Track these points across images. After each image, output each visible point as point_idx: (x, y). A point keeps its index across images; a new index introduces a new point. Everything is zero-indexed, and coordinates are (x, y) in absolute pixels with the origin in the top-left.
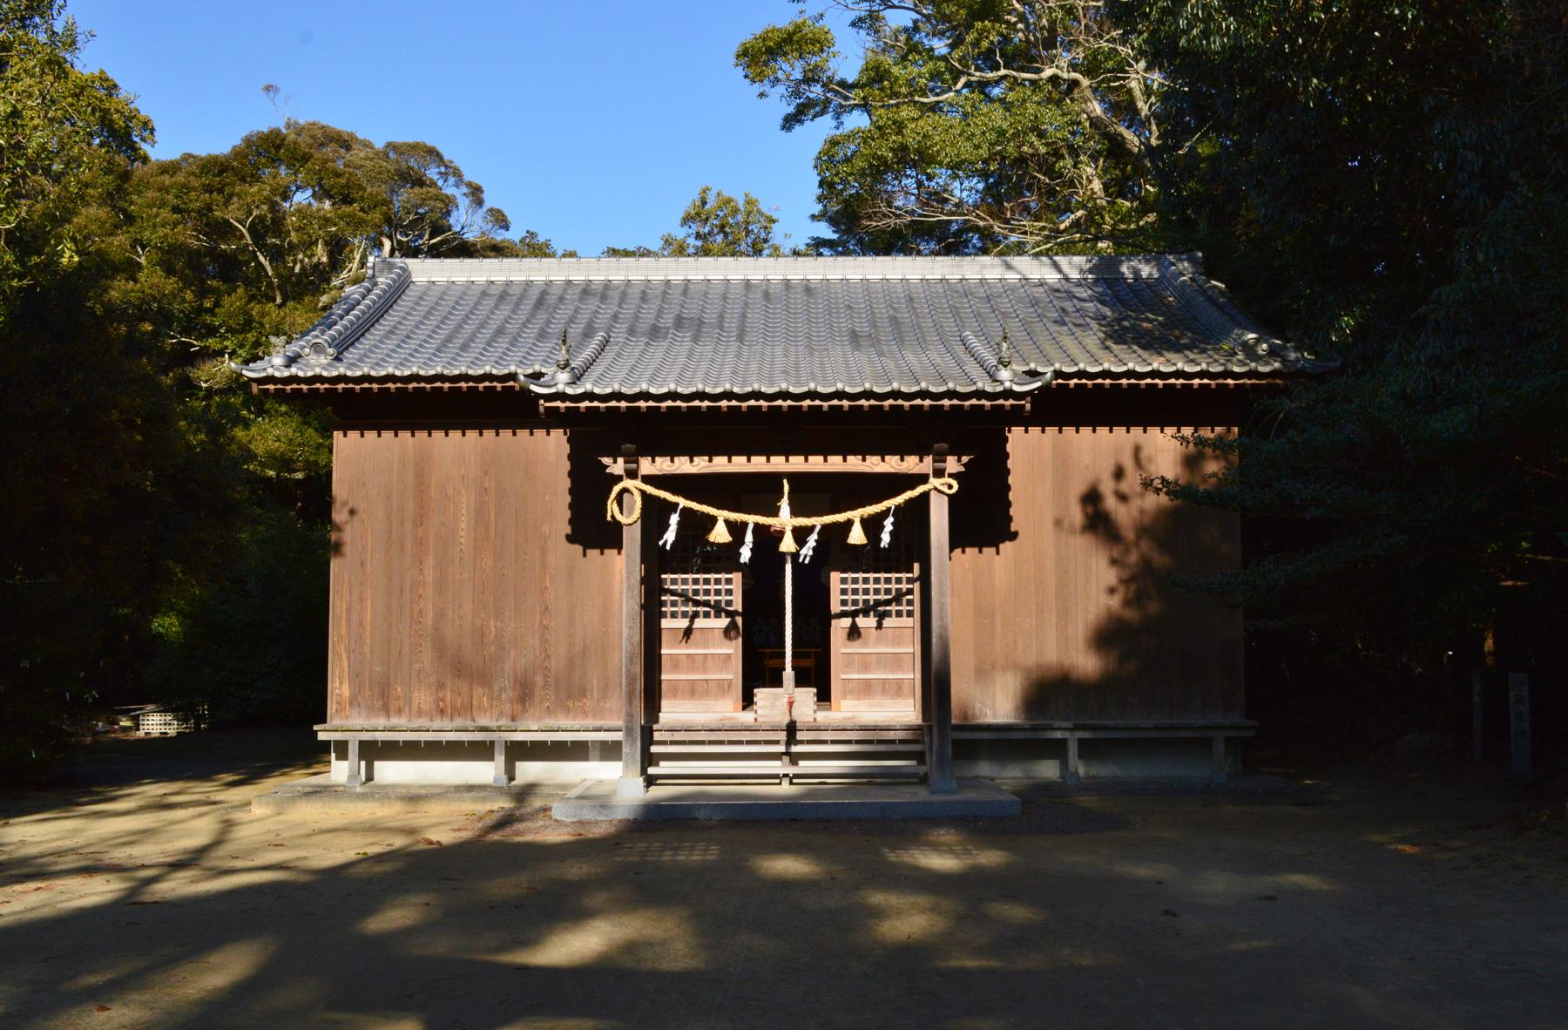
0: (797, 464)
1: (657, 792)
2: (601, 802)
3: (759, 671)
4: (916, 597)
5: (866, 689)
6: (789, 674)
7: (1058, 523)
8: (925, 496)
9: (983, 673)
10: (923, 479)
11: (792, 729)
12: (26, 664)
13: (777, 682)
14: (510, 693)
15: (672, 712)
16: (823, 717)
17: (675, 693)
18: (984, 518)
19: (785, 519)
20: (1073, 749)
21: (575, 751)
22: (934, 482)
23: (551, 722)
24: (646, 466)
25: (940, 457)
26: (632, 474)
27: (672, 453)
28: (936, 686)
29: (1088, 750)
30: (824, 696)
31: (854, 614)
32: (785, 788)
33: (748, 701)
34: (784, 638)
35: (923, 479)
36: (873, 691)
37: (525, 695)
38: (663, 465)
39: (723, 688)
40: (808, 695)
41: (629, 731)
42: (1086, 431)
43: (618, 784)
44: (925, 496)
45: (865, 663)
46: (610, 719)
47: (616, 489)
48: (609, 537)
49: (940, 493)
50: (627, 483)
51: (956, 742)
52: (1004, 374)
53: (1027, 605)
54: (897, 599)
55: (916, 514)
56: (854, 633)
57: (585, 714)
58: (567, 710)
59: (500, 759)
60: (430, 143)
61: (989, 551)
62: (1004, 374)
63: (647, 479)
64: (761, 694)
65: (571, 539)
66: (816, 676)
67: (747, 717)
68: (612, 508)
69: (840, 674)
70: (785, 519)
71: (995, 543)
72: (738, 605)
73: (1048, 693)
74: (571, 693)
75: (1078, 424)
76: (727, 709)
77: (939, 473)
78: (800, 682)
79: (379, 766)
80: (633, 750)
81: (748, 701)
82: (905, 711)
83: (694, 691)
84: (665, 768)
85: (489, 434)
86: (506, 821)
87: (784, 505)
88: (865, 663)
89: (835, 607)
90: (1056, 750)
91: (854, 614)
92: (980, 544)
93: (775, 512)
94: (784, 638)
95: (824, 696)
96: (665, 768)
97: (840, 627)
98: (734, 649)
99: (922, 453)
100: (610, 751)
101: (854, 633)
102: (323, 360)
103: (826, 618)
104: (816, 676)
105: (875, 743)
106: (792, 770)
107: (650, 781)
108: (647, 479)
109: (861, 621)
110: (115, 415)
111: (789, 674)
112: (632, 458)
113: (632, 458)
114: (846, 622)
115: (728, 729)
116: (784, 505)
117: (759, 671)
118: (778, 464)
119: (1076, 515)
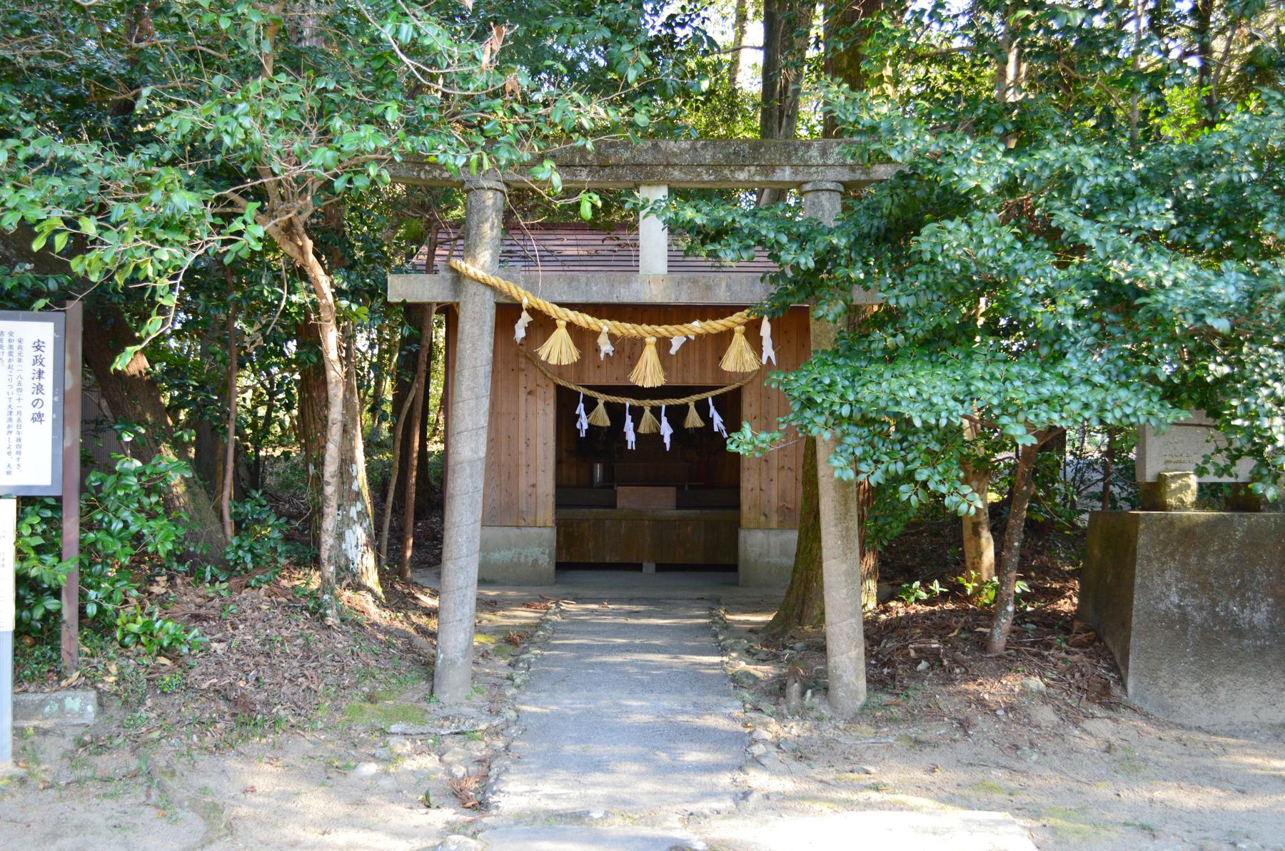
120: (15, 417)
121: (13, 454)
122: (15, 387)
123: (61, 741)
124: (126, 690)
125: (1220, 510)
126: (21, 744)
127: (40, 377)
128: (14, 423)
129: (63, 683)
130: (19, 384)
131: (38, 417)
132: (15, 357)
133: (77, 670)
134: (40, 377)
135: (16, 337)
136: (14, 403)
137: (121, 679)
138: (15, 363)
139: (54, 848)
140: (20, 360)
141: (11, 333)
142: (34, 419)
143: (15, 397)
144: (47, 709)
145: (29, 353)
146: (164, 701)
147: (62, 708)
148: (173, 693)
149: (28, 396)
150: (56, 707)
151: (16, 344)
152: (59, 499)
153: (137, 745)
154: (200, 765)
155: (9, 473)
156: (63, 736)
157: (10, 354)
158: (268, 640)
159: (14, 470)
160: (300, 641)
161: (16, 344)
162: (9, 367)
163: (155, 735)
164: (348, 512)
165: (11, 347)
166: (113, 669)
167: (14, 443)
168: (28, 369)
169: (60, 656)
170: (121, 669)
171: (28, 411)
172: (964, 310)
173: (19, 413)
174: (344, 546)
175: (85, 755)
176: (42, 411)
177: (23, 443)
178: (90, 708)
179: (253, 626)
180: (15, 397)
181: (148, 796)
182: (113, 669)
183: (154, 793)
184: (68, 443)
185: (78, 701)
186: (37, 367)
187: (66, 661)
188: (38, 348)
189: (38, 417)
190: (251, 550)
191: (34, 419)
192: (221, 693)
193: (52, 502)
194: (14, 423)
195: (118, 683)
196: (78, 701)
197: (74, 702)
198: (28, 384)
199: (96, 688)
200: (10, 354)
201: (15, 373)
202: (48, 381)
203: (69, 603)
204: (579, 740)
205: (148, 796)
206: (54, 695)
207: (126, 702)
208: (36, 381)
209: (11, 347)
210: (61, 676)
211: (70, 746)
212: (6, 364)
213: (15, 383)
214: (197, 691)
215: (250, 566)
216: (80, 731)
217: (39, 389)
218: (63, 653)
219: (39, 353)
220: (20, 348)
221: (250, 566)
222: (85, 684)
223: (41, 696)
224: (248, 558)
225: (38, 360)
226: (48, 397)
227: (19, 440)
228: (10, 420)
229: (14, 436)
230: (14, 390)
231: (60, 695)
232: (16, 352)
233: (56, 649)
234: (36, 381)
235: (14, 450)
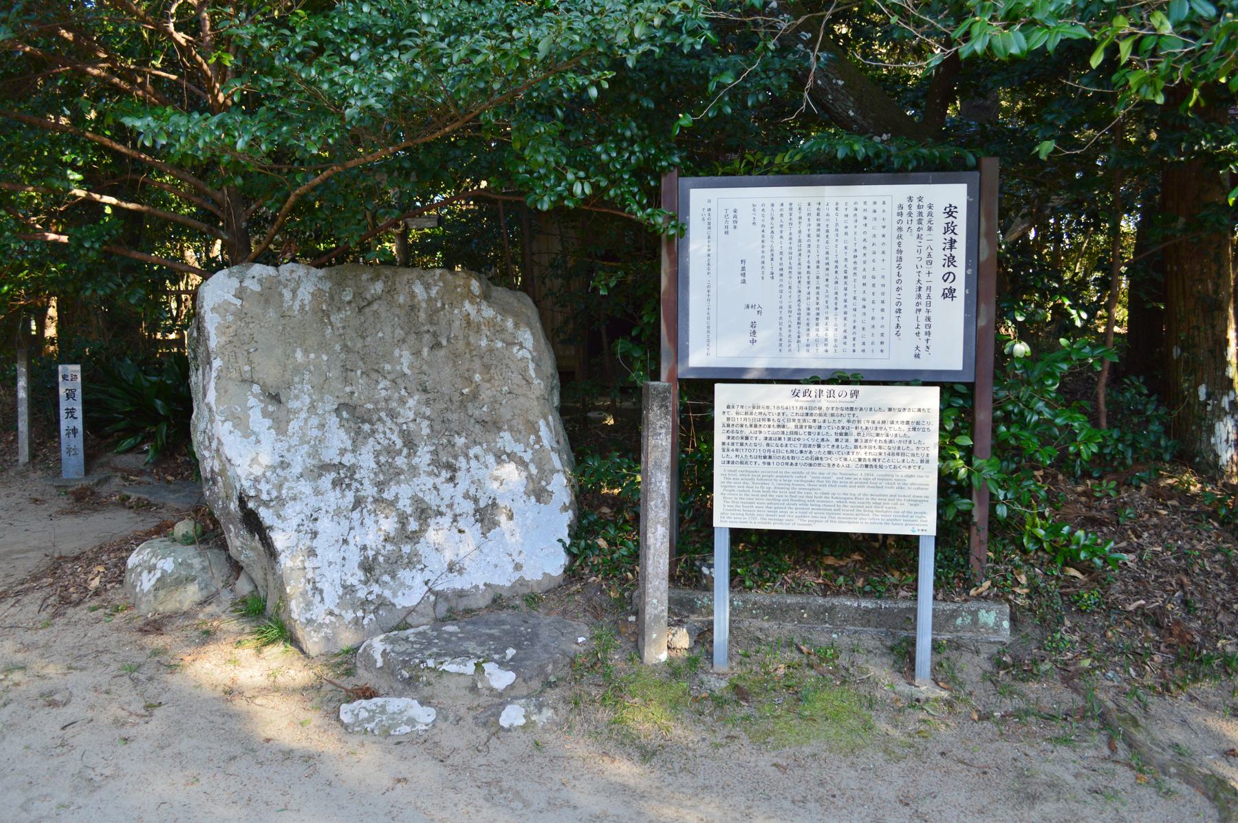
120: (924, 293)
121: (922, 333)
122: (925, 259)
123: (976, 659)
124: (1040, 605)
125: (1227, 318)
126: (938, 658)
127: (951, 248)
128: (924, 300)
129: (973, 592)
130: (929, 255)
131: (949, 293)
132: (925, 225)
133: (987, 578)
134: (951, 248)
135: (925, 203)
136: (924, 277)
137: (1034, 590)
138: (924, 232)
139: (1035, 815)
140: (930, 229)
141: (920, 199)
142: (945, 296)
143: (924, 271)
144: (959, 621)
145: (940, 220)
146: (1082, 621)
147: (975, 621)
148: (1093, 612)
149: (939, 270)
150: (968, 620)
151: (925, 211)
152: (971, 386)
153: (1068, 676)
154: (1153, 709)
155: (917, 356)
156: (978, 652)
157: (920, 222)
158: (1181, 555)
159: (923, 353)
160: (1218, 557)
161: (925, 211)
162: (918, 237)
163: (1086, 663)
164: (1220, 402)
165: (920, 214)
166: (1023, 579)
167: (923, 323)
168: (938, 239)
169: (968, 562)
170: (1029, 579)
171: (939, 286)
172: (612, 193)
173: (929, 288)
174: (1213, 440)
175: (1008, 679)
176: (954, 285)
177: (933, 322)
178: (1006, 624)
179: (1159, 535)
180: (924, 271)
181: (1113, 749)
182: (1023, 579)
183: (1122, 752)
184: (982, 322)
185: (993, 614)
186: (948, 236)
187: (975, 567)
188: (950, 214)
189: (949, 293)
190: (1133, 445)
191: (945, 296)
192: (1155, 619)
193: (963, 389)
194: (924, 300)
195: (1029, 596)
196: (993, 614)
197: (988, 616)
198: (939, 256)
199: (1008, 601)
200: (920, 222)
201: (925, 244)
202: (960, 252)
203: (980, 503)
204: (56, 233)
205: (1113, 749)
206: (966, 605)
207: (1043, 620)
208: (948, 252)
209: (920, 214)
210: (968, 584)
211: (988, 666)
212: (915, 233)
213: (924, 255)
214: (1121, 612)
215: (1129, 462)
216: (995, 649)
217: (951, 260)
218: (972, 558)
219: (951, 219)
220: (930, 214)
221: (1129, 462)
222: (996, 595)
223: (952, 606)
224: (1129, 453)
225: (950, 228)
226: (960, 270)
227: (929, 319)
228: (919, 296)
229: (923, 315)
230: (923, 263)
231: (973, 605)
232: (925, 219)
233: (966, 553)
234: (948, 252)
235: (923, 330)
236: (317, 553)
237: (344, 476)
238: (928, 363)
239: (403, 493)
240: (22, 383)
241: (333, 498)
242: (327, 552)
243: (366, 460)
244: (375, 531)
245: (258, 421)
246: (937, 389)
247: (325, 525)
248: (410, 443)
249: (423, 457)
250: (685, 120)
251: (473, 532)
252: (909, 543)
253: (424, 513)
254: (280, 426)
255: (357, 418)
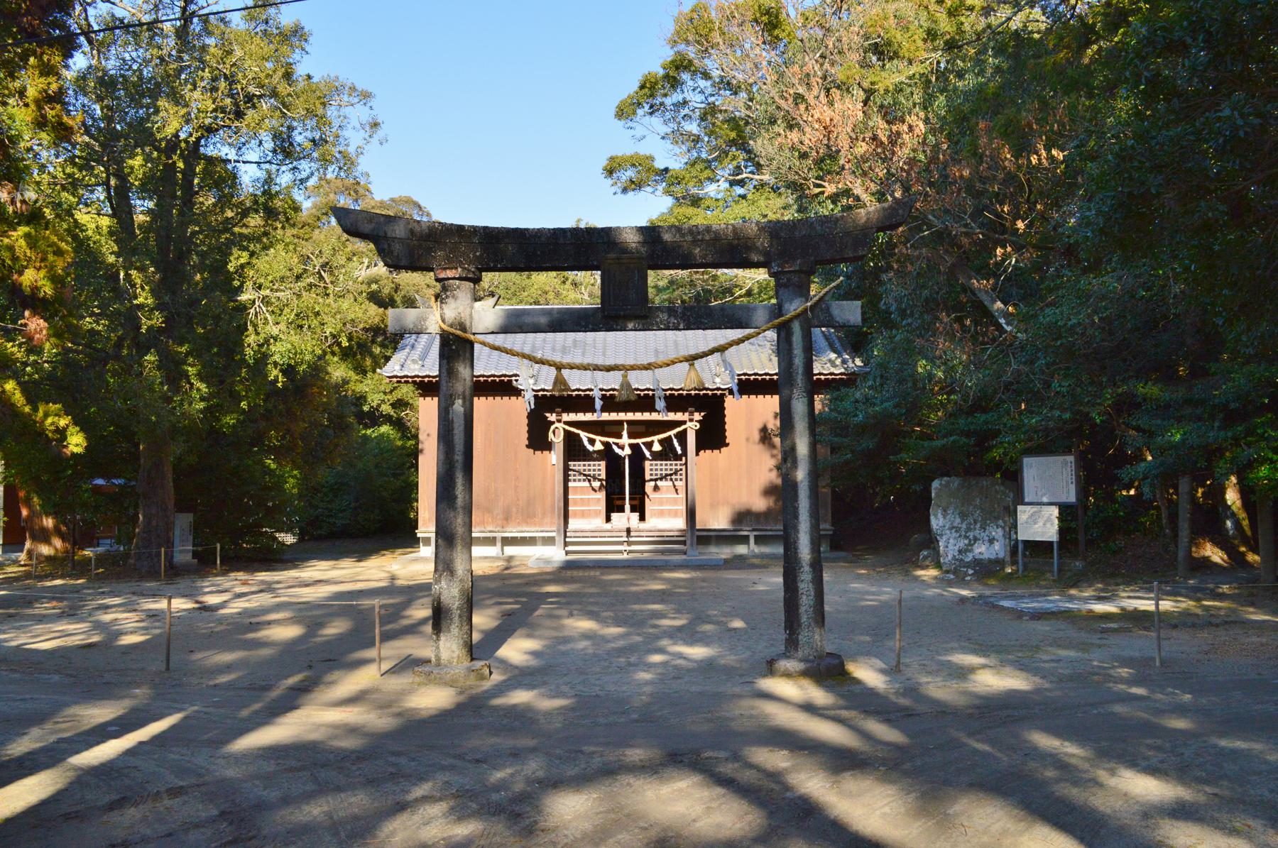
0: (630, 416)
1: (570, 557)
2: (548, 561)
3: (613, 506)
4: (683, 472)
5: (661, 514)
6: (627, 507)
7: (748, 439)
8: (685, 430)
9: (714, 506)
10: (684, 422)
11: (628, 531)
12: (270, 504)
13: (621, 510)
14: (501, 516)
15: (574, 524)
16: (642, 526)
17: (575, 515)
18: (712, 436)
19: (625, 440)
20: (752, 540)
21: (531, 541)
22: (689, 424)
23: (520, 529)
24: (565, 417)
25: (691, 413)
26: (559, 421)
27: (576, 411)
28: (691, 514)
29: (760, 540)
30: (642, 518)
31: (656, 480)
32: (625, 556)
33: (608, 519)
34: (624, 489)
35: (684, 422)
36: (664, 515)
37: (507, 518)
38: (572, 417)
39: (597, 513)
40: (636, 516)
41: (558, 531)
42: (760, 397)
43: (556, 554)
44: (685, 430)
45: (661, 502)
46: (550, 528)
47: (553, 427)
48: (548, 446)
49: (692, 428)
50: (557, 425)
51: (698, 537)
52: (718, 380)
53: (735, 477)
54: (675, 473)
55: (682, 437)
56: (656, 488)
57: (535, 525)
58: (527, 524)
59: (499, 544)
60: (415, 199)
61: (716, 452)
62: (718, 380)
63: (566, 423)
64: (614, 516)
65: (528, 446)
66: (639, 508)
67: (608, 526)
68: (551, 435)
69: (649, 507)
70: (625, 440)
71: (719, 448)
72: (603, 476)
73: (742, 517)
74: (528, 516)
75: (757, 394)
76: (598, 522)
77: (691, 420)
78: (633, 510)
79: (506, 548)
80: (560, 540)
81: (608, 519)
82: (679, 523)
83: (583, 514)
84: (570, 548)
85: (490, 399)
86: (507, 569)
87: (625, 433)
88: (661, 502)
89: (647, 477)
90: (745, 540)
91: (656, 480)
92: (712, 448)
93: (620, 437)
94: (624, 489)
95: (642, 518)
96: (570, 548)
97: (649, 486)
98: (602, 496)
99: (684, 411)
100: (549, 541)
101: (656, 488)
102: (417, 367)
103: (644, 482)
104: (639, 508)
105: (664, 540)
106: (628, 548)
107: (567, 553)
108: (566, 423)
109: (659, 483)
110: (316, 390)
111: (627, 507)
112: (559, 414)
113: (559, 414)
114: (652, 484)
115: (595, 527)
116: (625, 433)
117: (613, 506)
118: (622, 416)
119: (757, 436)
236: (949, 546)
237: (958, 530)
238: (1028, 508)
239: (971, 535)
240: (1223, 743)
241: (954, 535)
242: (951, 547)
243: (964, 526)
244: (963, 543)
245: (940, 516)
246: (476, 399)
247: (951, 541)
248: (975, 522)
249: (978, 525)
250: (100, 482)
251: (987, 544)
252: (1051, 543)
253: (976, 539)
254: (944, 517)
255: (963, 516)
